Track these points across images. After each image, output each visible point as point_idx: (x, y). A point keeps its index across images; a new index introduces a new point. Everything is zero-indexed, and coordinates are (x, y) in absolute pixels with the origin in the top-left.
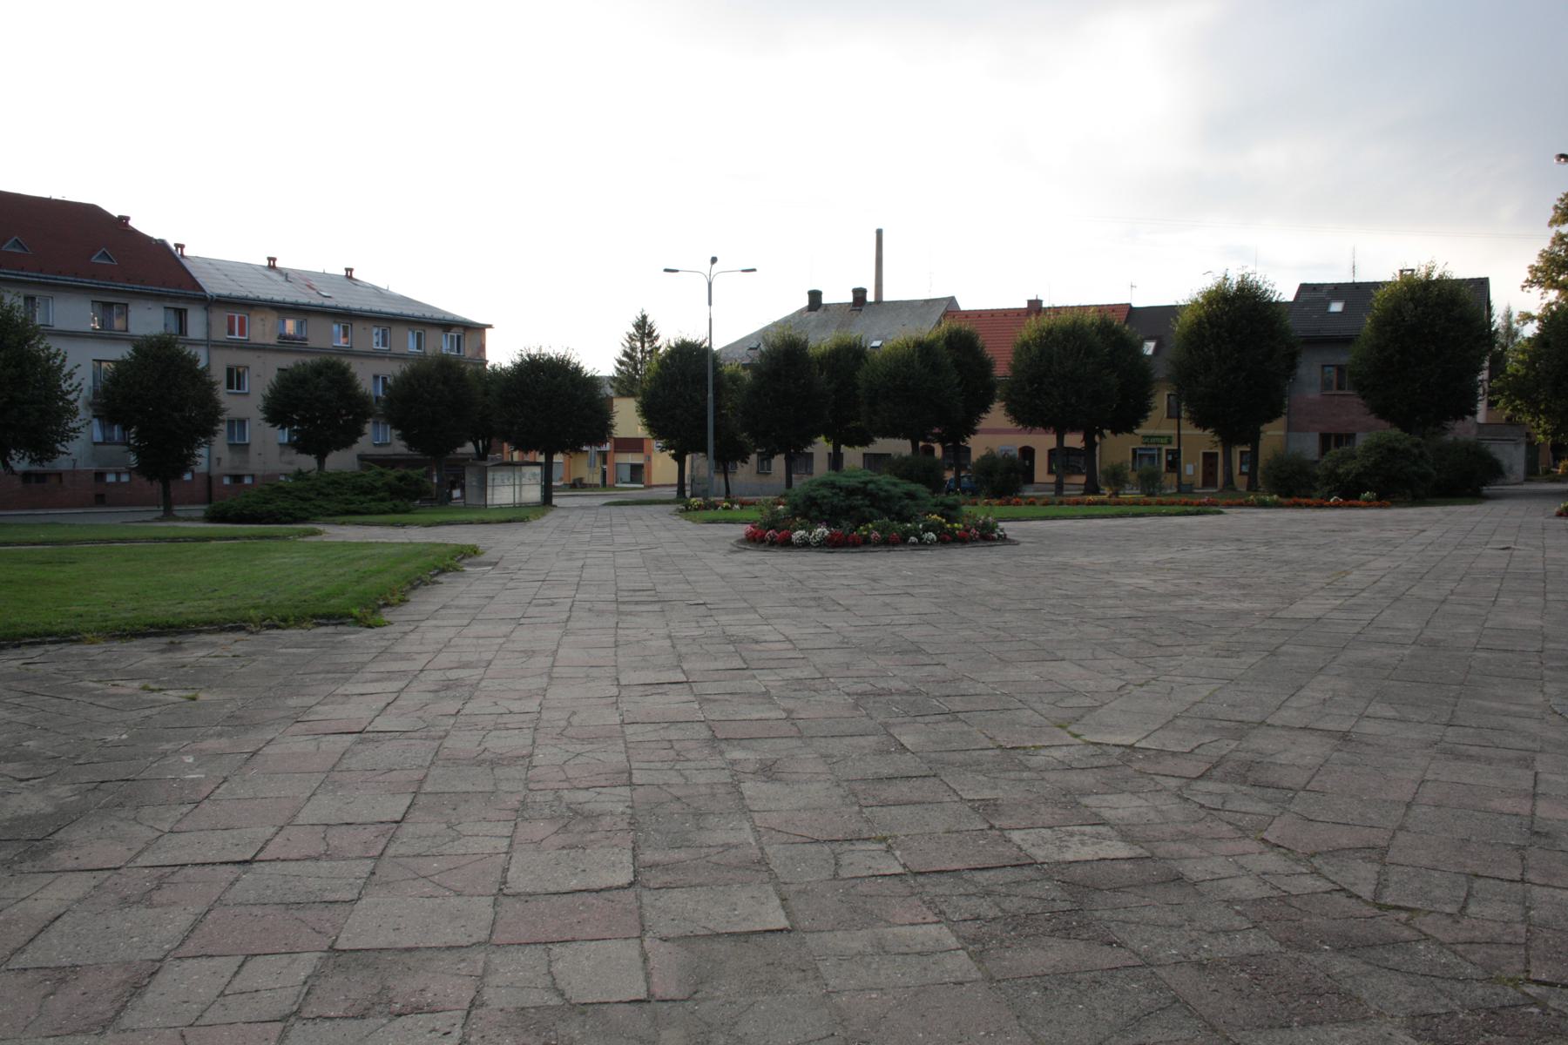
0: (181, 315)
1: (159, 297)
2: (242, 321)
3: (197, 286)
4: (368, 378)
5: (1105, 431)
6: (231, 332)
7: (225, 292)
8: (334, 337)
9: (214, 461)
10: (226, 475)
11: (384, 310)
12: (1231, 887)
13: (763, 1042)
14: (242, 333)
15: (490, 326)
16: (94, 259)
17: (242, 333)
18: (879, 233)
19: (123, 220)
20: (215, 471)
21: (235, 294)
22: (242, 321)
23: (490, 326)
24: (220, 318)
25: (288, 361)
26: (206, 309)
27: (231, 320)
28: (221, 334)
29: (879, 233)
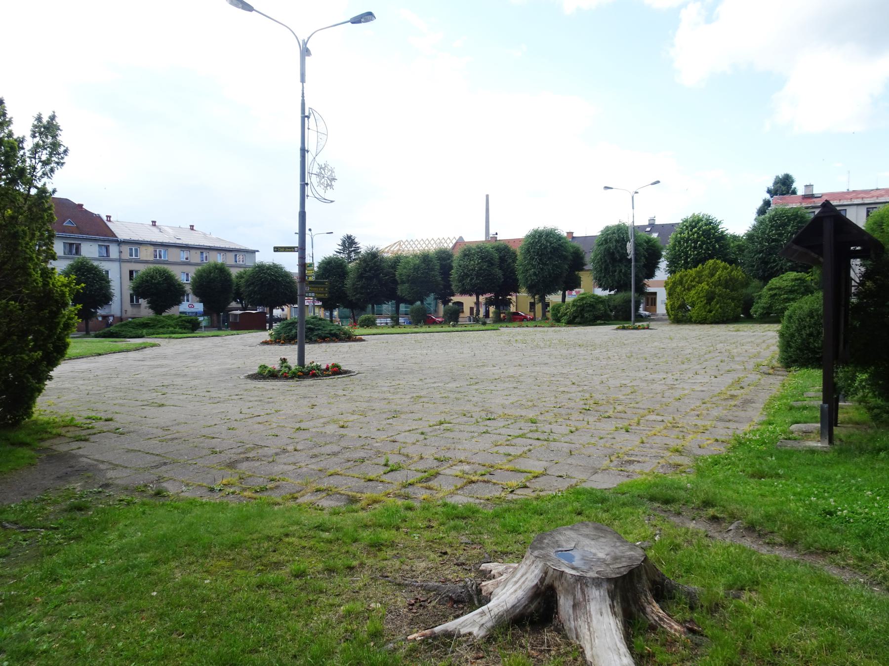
0: (107, 248)
1: (95, 240)
2: (136, 250)
3: (114, 235)
4: (184, 276)
5: (141, 301)
6: (131, 255)
7: (128, 238)
8: (219, 259)
9: (123, 311)
10: (535, 315)
11: (206, 244)
12: (420, 653)
13: (885, 416)
14: (136, 256)
15: (258, 251)
16: (64, 224)
17: (136, 256)
18: (487, 196)
19: (81, 206)
20: (124, 316)
21: (133, 239)
22: (136, 250)
23: (258, 251)
24: (126, 249)
25: (200, 268)
26: (119, 245)
27: (131, 249)
28: (126, 256)
29: (487, 196)
